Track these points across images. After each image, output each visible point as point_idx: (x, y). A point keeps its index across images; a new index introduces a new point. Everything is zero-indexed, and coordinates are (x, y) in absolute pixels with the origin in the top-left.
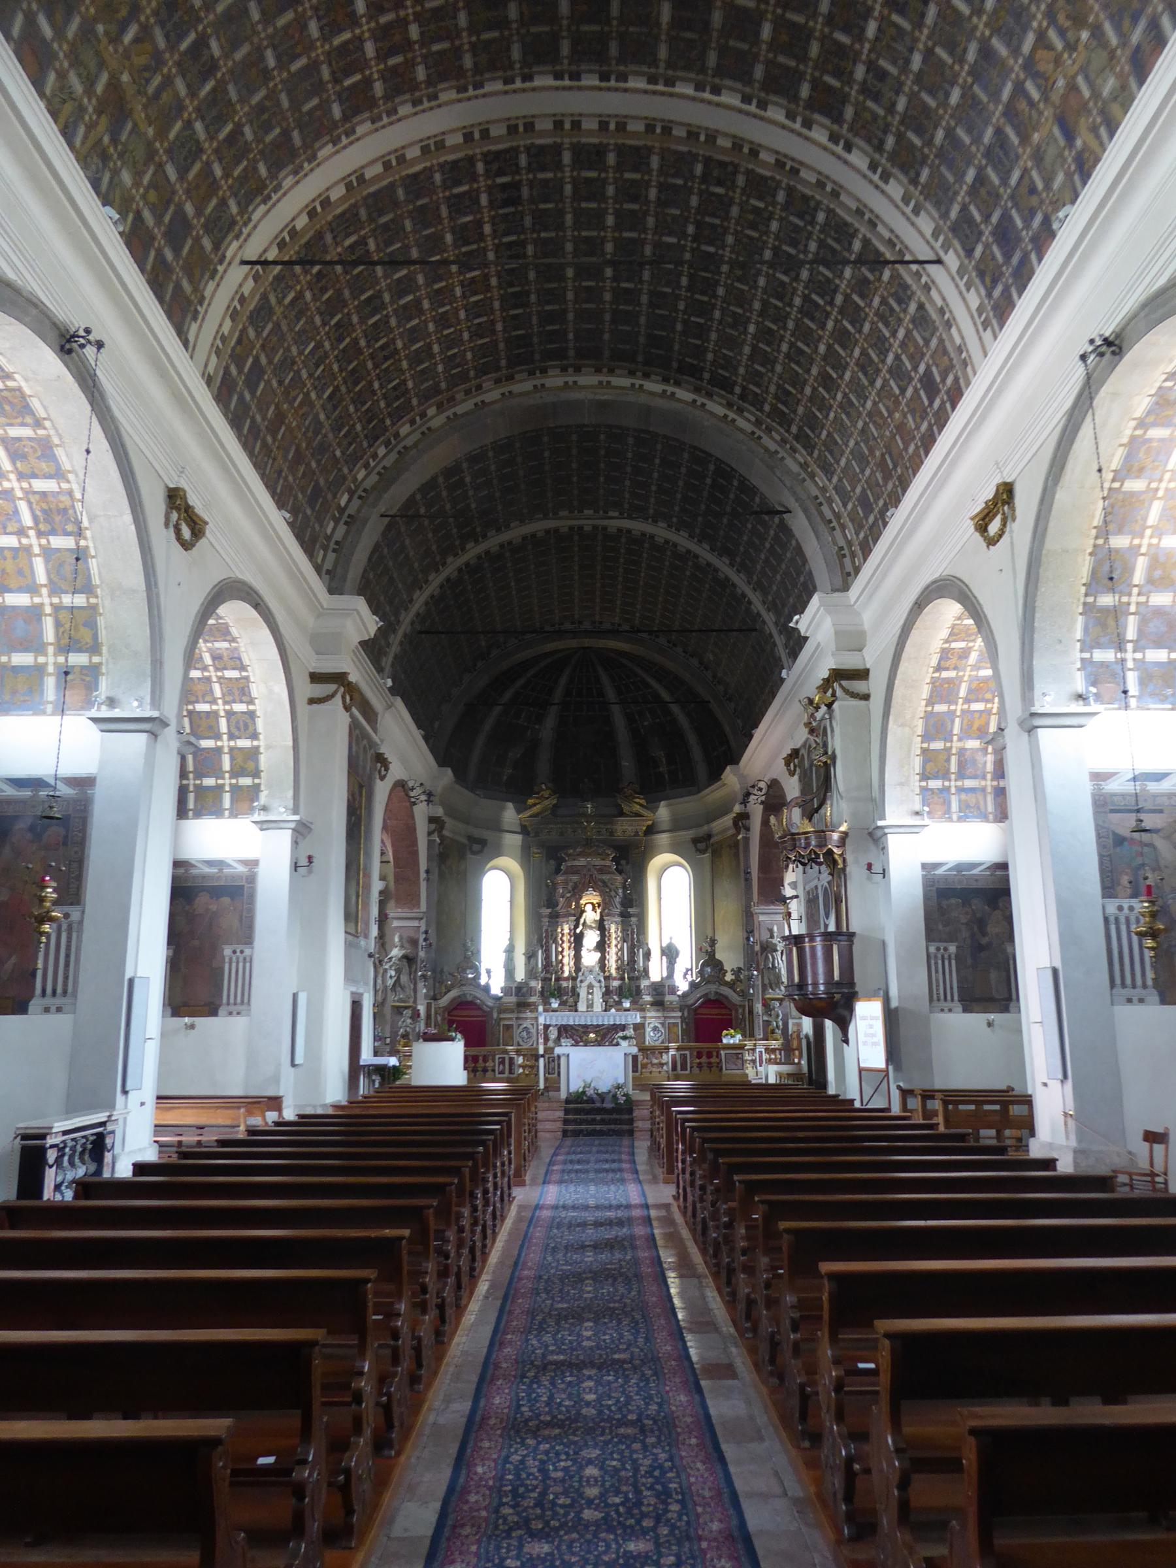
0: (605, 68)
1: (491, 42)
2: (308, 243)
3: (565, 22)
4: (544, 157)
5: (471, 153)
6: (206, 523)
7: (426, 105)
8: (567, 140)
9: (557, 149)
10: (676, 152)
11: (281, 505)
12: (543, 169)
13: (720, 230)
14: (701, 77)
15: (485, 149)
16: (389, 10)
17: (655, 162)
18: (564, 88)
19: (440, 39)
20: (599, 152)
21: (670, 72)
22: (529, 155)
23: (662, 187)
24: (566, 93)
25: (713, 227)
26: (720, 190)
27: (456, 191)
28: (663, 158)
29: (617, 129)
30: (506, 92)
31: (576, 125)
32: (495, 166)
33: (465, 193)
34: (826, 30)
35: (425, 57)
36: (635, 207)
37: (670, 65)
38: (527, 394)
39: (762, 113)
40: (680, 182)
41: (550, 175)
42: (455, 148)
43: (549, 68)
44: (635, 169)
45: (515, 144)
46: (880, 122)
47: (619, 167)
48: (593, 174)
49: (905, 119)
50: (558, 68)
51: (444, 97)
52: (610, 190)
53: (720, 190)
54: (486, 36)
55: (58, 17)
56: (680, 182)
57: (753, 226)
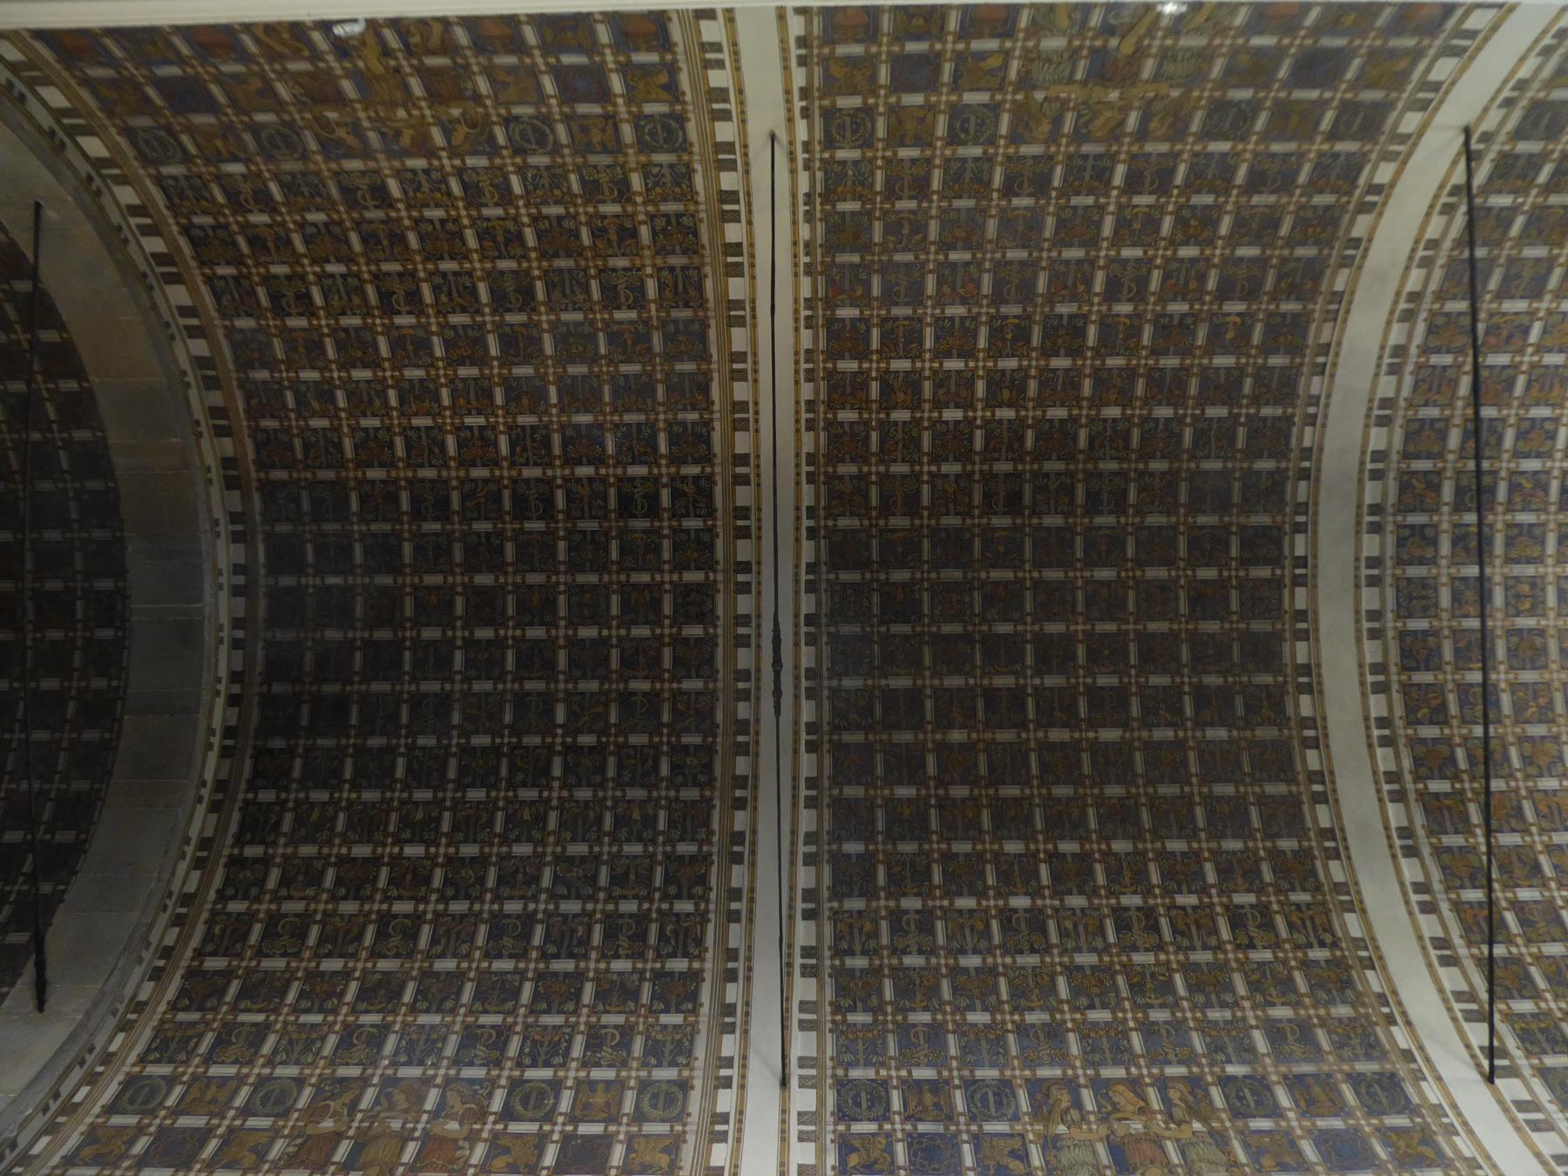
0: (824, 620)
1: (866, 496)
2: (696, 233)
3: (882, 576)
4: (697, 549)
5: (718, 461)
7: (804, 416)
8: (720, 577)
9: (709, 565)
10: (712, 710)
12: (676, 548)
13: (598, 779)
14: (826, 728)
15: (718, 479)
16: (935, 393)
18: (797, 575)
19: (882, 442)
20: (704, 616)
21: (826, 693)
25: (602, 769)
26: (665, 770)
30: (798, 508)
35: (867, 423)
37: (835, 693)
38: (210, 511)
39: (802, 804)
41: (666, 556)
42: (729, 443)
43: (823, 557)
45: (719, 514)
46: (872, 943)
49: (312, 976)
50: (824, 568)
53: (665, 770)
54: (874, 491)
55: (1403, 64)
56: (666, 718)
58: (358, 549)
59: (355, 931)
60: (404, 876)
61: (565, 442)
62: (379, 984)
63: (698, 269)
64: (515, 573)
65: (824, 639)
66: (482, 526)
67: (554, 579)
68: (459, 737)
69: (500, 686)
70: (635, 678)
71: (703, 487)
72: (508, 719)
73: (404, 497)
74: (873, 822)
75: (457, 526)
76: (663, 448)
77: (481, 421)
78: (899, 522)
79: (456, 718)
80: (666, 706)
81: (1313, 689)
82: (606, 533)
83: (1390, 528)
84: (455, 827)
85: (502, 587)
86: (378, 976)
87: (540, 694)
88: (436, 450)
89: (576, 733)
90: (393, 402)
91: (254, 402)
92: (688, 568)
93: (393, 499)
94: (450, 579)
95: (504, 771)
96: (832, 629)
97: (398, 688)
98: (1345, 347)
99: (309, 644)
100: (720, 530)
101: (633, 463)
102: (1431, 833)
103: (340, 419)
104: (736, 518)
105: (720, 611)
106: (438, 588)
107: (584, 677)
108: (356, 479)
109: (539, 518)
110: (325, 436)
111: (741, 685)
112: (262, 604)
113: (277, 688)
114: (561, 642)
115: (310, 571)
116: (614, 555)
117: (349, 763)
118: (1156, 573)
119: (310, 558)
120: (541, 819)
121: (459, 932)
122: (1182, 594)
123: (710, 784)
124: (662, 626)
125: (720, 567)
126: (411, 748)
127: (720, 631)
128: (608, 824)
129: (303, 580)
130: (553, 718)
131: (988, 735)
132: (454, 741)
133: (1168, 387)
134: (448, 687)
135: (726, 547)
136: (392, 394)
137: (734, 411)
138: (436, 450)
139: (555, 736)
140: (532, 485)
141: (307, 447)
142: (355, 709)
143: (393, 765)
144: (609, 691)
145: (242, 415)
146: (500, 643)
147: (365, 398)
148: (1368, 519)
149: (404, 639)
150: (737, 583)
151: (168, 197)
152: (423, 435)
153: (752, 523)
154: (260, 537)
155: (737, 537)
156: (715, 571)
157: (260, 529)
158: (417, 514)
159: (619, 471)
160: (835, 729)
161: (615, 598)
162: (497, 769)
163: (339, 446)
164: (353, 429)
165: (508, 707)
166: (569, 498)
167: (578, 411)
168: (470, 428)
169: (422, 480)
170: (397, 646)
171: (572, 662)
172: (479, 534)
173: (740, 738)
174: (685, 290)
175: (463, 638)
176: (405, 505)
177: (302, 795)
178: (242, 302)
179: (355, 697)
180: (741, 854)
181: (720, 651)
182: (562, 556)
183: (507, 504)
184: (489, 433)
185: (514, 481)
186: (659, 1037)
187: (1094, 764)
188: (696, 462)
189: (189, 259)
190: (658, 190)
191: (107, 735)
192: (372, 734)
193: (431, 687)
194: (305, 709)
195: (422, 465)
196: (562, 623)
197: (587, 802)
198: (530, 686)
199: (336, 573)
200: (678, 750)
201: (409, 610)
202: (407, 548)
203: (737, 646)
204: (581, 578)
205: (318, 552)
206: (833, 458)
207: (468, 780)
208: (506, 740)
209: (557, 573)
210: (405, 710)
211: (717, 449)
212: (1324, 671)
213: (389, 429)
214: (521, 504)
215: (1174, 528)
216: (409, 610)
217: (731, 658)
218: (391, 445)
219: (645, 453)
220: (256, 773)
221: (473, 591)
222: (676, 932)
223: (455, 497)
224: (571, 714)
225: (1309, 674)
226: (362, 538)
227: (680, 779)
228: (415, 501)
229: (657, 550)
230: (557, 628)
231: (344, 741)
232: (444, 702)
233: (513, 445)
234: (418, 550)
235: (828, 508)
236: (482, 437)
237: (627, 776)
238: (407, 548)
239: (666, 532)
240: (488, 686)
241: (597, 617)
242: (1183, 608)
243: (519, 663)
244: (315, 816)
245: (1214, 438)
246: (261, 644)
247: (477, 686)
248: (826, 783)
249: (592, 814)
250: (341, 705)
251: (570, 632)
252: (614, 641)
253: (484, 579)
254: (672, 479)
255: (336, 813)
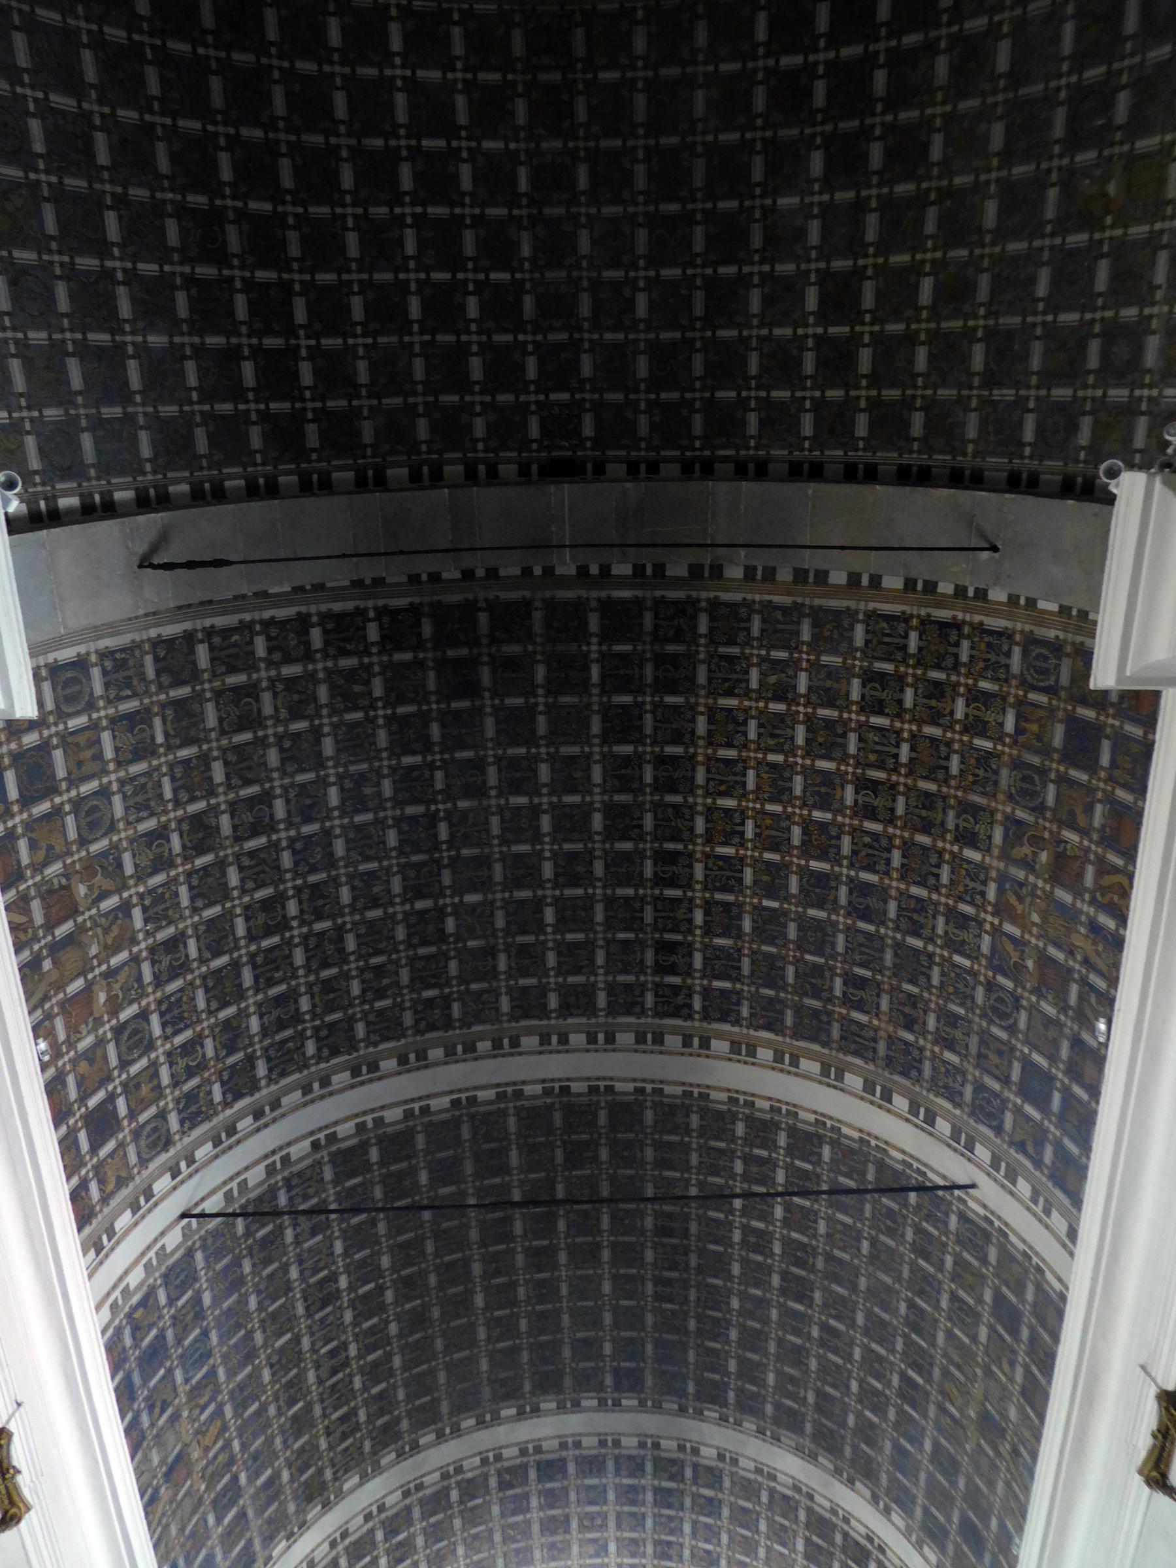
0: (565, 1099)
3: (603, 1141)
5: (705, 1025)
6: (28, 1509)
8: (602, 1020)
9: (612, 1010)
10: (483, 1022)
11: (1098, 1057)
12: (628, 987)
14: (473, 1110)
15: (689, 1023)
17: (505, 1004)
20: (566, 1009)
21: (502, 1106)
22: (643, 1004)
23: (494, 974)
24: (601, 1074)
25: (424, 943)
26: (428, 994)
27: (727, 985)
28: (497, 1010)
29: (549, 1035)
31: (592, 1039)
32: (680, 1000)
33: (718, 978)
34: (104, 723)
36: (521, 939)
40: (474, 986)
42: (720, 1036)
44: (525, 990)
45: (657, 1021)
47: (543, 991)
48: (572, 979)
51: (724, 1096)
52: (551, 959)
53: (428, 994)
54: (675, 1138)
56: (474, 986)
57: (379, 970)
58: (626, 699)
59: (251, 776)
60: (310, 796)
61: (727, 906)
62: (207, 827)
63: (873, 1060)
64: (604, 850)
65: (549, 1101)
66: (648, 821)
67: (599, 884)
68: (446, 811)
69: (496, 842)
70: (509, 957)
71: (681, 1010)
72: (465, 852)
73: (678, 750)
74: (396, 1161)
75: (648, 798)
76: (717, 984)
77: (749, 835)
78: (649, 1153)
79: (463, 804)
80: (485, 985)
81: (521, 1415)
82: (641, 929)
83: (642, 1452)
84: (359, 828)
85: (590, 839)
86: (213, 822)
87: (490, 878)
88: (723, 788)
89: (456, 914)
90: (771, 757)
91: (779, 615)
92: (609, 994)
93: (677, 739)
94: (597, 790)
95: (416, 858)
96: (557, 1106)
97: (490, 745)
98: (776, 1449)
99: (530, 648)
100: (642, 1020)
101: (705, 958)
102: (420, 1501)
103: (757, 700)
104: (654, 1033)
105: (570, 1021)
106: (589, 778)
107: (507, 915)
108: (697, 704)
109: (655, 873)
110: (740, 681)
111: (506, 1042)
112: (570, 594)
113: (483, 618)
114: (540, 893)
115: (604, 648)
116: (621, 936)
117: (412, 709)
118: (608, 1318)
119: (618, 648)
120: (375, 903)
121: (263, 872)
122: (592, 1334)
123: (419, 1032)
124: (556, 976)
125: (610, 1020)
126: (432, 767)
127: (553, 1022)
128: (376, 960)
129: (595, 640)
130: (469, 892)
131: (473, 1224)
132: (441, 807)
133: (753, 1340)
134: (493, 793)
135: (629, 1025)
136: (780, 758)
137: (748, 1045)
138: (723, 788)
139: (452, 897)
140: (688, 870)
141: (730, 659)
142: (466, 704)
143: (413, 753)
144: (496, 937)
145: (767, 597)
146: (537, 837)
147: (777, 732)
148: (649, 1441)
149: (538, 746)
150: (596, 1033)
151: (991, 633)
152: (738, 778)
153: (649, 1047)
154: (639, 593)
155: (637, 1033)
156: (606, 1016)
157: (648, 594)
158: (661, 761)
159: (698, 946)
160: (472, 1117)
161: (581, 936)
162: (418, 851)
163: (729, 693)
164: (746, 710)
165: (476, 851)
166: (675, 901)
167: (754, 921)
168: (742, 824)
169: (694, 769)
170: (531, 740)
171: (522, 902)
172: (641, 818)
173: (460, 1048)
174: (855, 1042)
175: (540, 804)
176: (669, 750)
177: (377, 669)
178: (881, 643)
179: (478, 703)
180: (360, 1075)
181: (535, 1022)
182: (620, 892)
183: (670, 846)
184: (737, 840)
185: (691, 855)
186: (125, 435)
187: (455, 1295)
188: (704, 1008)
189: (929, 610)
190: (943, 1070)
191: (424, 447)
192: (443, 726)
193: (492, 776)
194: (464, 652)
195: (708, 771)
196: (557, 893)
197: (393, 938)
198: (498, 868)
199: (603, 676)
200: (447, 1001)
201: (568, 750)
202: (628, 749)
203: (541, 1035)
204: (599, 909)
205: (623, 656)
206: (704, 1112)
207: (405, 827)
208: (445, 854)
209: (604, 887)
210: (468, 754)
211: (715, 1026)
212: (535, 1420)
213: (745, 746)
214: (672, 858)
215: (643, 1329)
216: (568, 750)
217: (529, 1032)
218: (729, 745)
219: (713, 969)
220: (394, 613)
221: (586, 812)
222: (289, 1050)
223: (677, 799)
224: (473, 907)
225: (532, 1411)
226: (637, 705)
227: (420, 1008)
228: (674, 760)
229: (625, 971)
230: (553, 889)
231: (433, 698)
232: (478, 791)
233: (725, 858)
234: (627, 760)
235: (662, 1104)
236: (735, 832)
237: (419, 965)
238: (628, 749)
239: (642, 978)
240: (496, 830)
241: (563, 922)
242: (579, 1335)
243: (519, 856)
244: (357, 688)
245: (712, 1359)
246: (527, 594)
247: (495, 821)
248: (426, 1120)
249: (383, 945)
250: (471, 689)
251: (549, 900)
252: (542, 938)
253: (597, 822)
254: (690, 988)
255: (362, 708)
